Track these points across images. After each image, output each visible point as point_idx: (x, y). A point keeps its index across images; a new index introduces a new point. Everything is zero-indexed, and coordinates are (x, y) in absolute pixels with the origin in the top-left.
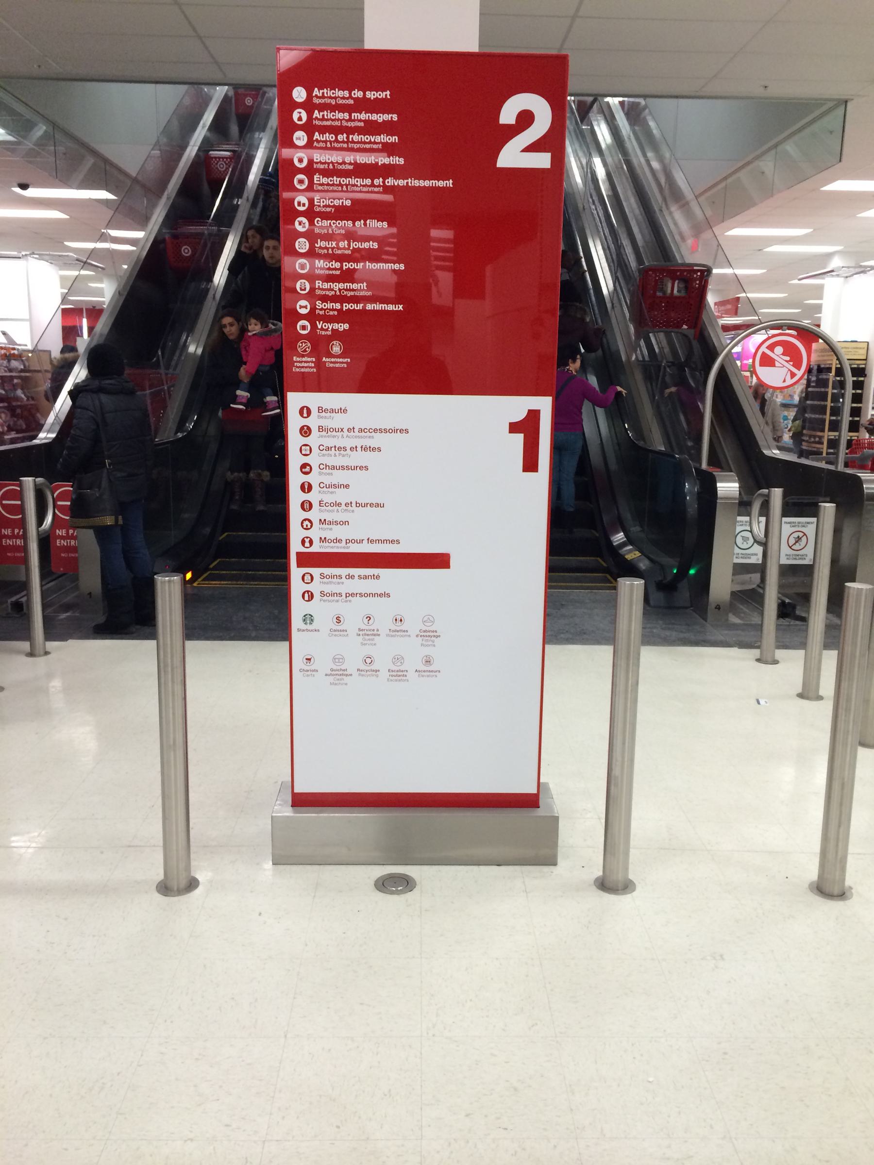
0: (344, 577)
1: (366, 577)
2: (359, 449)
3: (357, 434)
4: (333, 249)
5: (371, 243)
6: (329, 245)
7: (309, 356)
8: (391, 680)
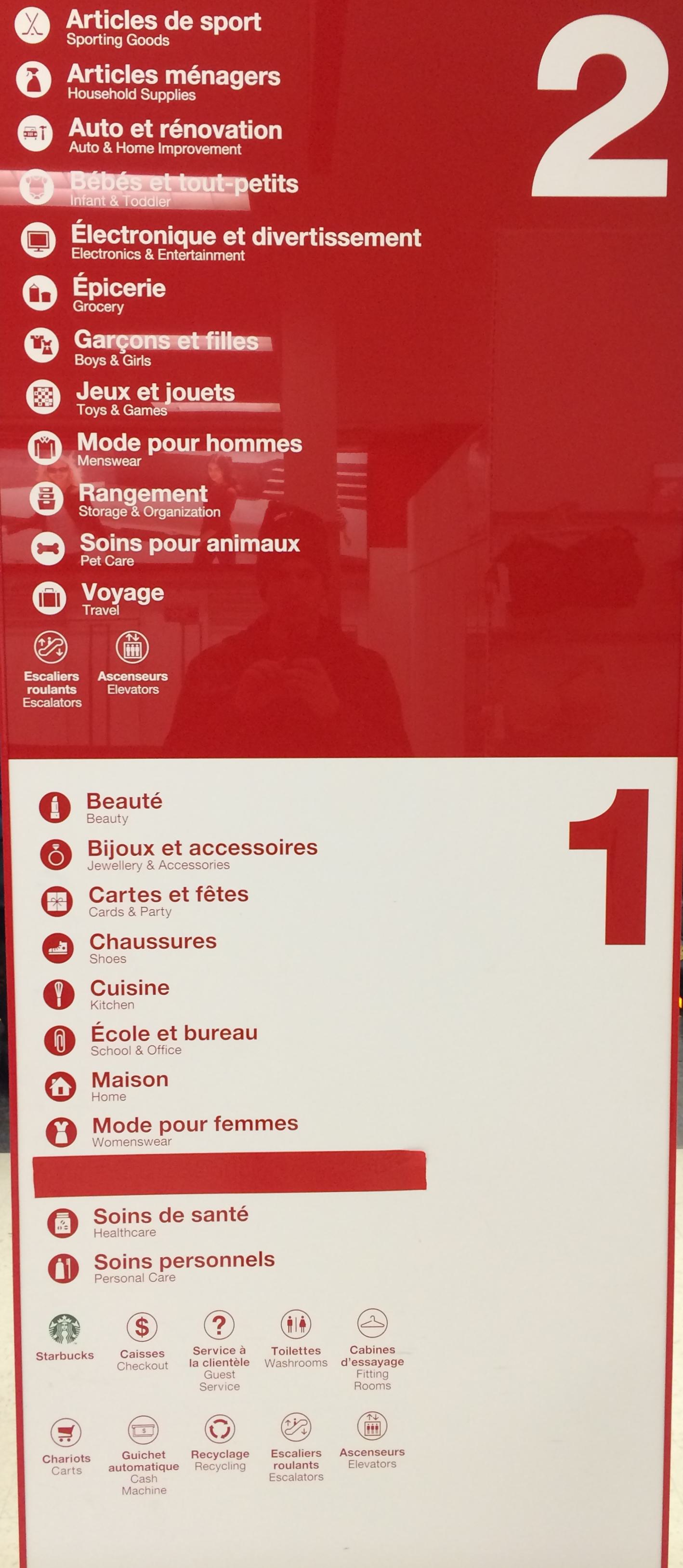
0: (155, 1217)
1: (212, 1216)
2: (192, 895)
3: (186, 857)
4: (121, 404)
5: (218, 388)
6: (111, 394)
7: (64, 668)
8: (280, 1478)
